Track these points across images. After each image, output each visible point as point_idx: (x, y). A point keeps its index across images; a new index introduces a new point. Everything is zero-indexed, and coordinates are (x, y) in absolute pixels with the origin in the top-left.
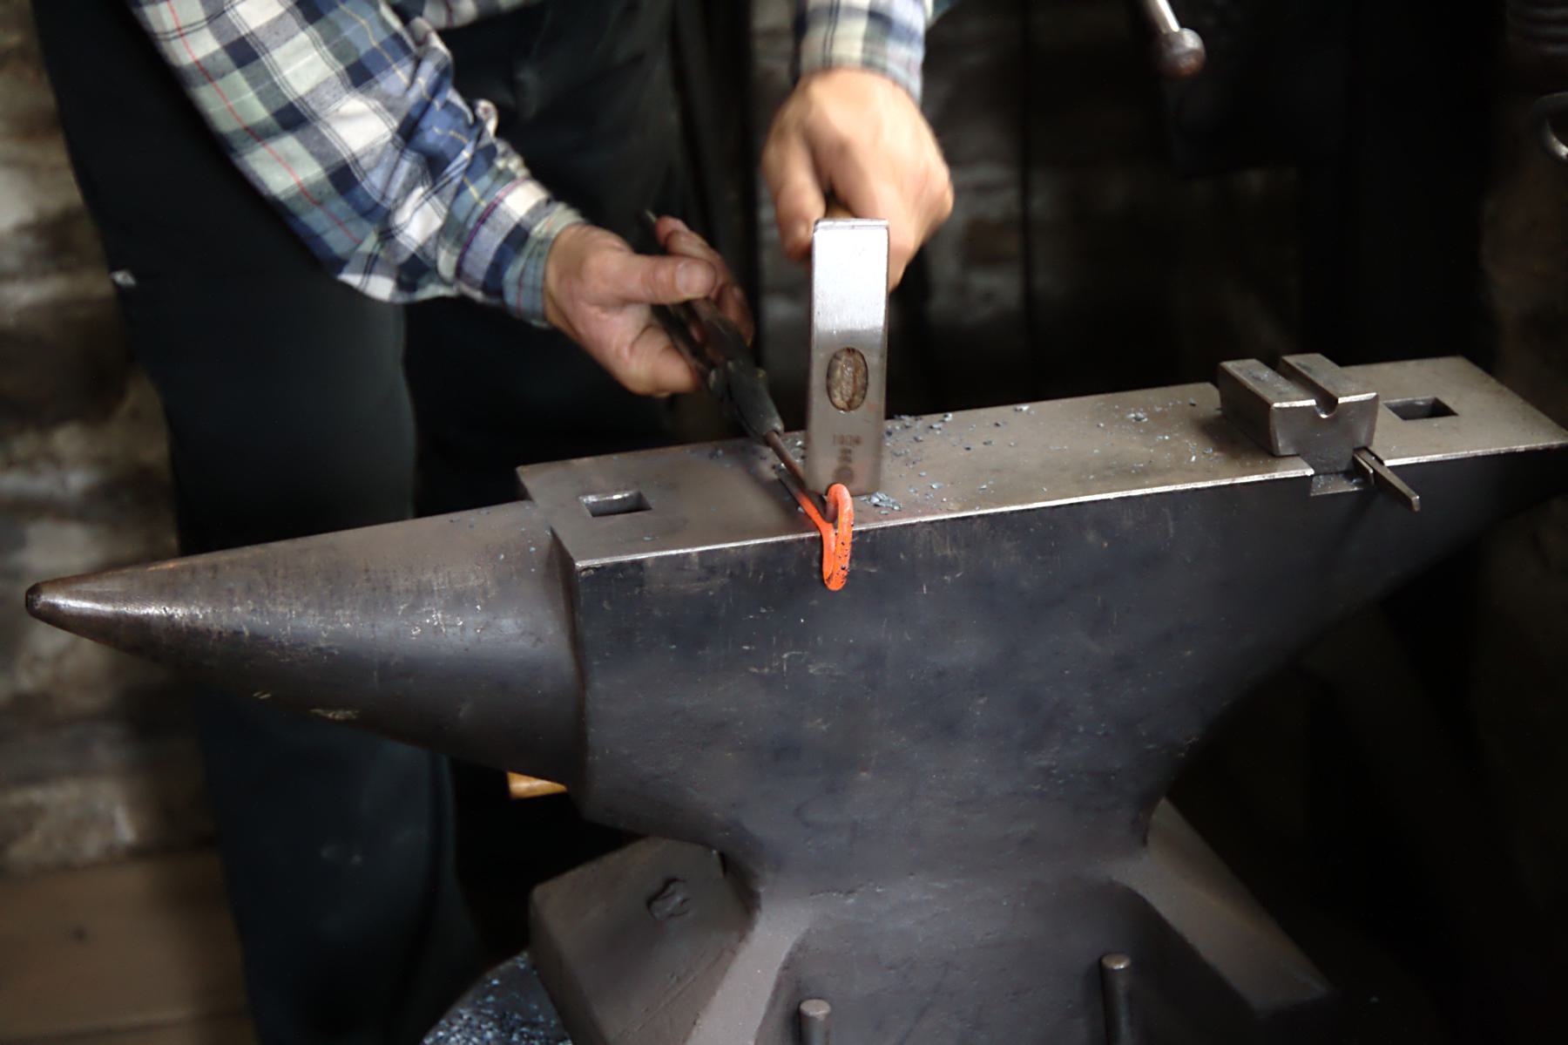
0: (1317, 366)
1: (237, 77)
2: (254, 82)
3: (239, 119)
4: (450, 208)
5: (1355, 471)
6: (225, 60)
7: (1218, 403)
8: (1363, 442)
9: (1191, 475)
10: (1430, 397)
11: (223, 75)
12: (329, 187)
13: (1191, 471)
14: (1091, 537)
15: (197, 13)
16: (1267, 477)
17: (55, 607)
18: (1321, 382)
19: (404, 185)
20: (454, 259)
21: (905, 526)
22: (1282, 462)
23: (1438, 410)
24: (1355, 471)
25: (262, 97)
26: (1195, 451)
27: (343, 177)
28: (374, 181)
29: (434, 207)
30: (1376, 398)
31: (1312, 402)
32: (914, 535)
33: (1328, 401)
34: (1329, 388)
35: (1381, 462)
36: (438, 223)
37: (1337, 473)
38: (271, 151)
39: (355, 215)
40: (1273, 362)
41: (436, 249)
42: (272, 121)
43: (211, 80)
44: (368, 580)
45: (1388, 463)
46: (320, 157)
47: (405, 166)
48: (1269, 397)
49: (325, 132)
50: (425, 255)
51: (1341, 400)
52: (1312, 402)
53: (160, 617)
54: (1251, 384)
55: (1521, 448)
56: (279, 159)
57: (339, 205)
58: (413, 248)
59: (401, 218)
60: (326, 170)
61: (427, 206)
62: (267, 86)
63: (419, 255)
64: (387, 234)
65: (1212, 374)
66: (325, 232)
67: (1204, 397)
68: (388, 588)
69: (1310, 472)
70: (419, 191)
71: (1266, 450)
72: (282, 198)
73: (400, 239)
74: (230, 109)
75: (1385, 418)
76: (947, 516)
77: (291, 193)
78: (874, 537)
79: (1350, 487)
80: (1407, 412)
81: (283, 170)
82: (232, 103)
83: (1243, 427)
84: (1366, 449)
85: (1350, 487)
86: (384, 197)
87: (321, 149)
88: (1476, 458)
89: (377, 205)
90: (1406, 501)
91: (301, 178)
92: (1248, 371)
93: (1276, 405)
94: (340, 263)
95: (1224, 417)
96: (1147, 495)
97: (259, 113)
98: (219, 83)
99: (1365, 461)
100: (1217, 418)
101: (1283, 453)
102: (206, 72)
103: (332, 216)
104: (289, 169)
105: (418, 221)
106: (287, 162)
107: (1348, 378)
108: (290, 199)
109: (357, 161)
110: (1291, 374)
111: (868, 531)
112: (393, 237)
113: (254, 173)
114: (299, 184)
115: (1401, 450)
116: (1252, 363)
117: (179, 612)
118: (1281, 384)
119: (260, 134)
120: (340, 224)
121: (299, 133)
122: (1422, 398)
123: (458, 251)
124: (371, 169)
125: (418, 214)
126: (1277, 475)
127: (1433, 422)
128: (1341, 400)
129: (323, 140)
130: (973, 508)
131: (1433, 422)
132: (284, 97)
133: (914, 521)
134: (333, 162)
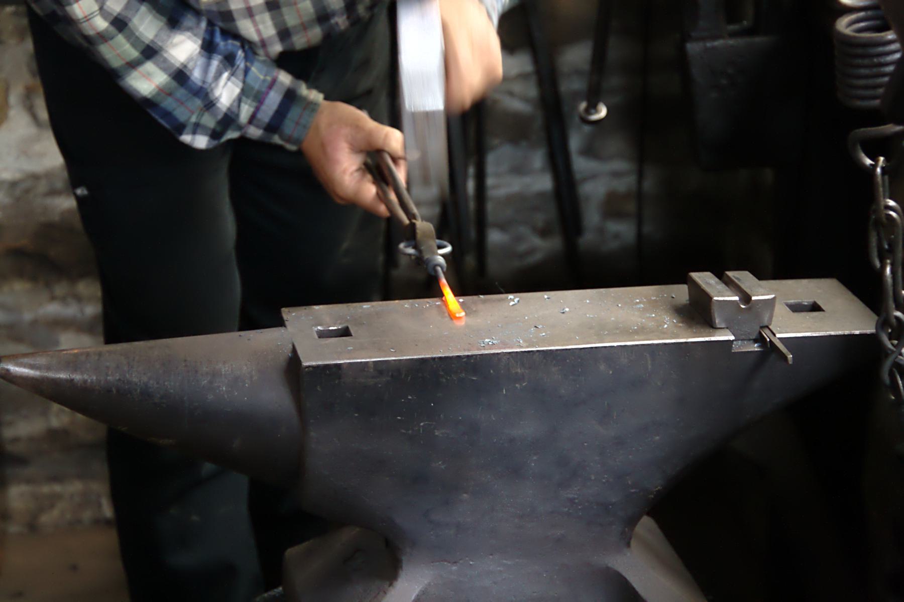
0: (745, 278)
1: (120, 38)
2: (128, 38)
3: (123, 59)
4: (244, 82)
5: (760, 339)
6: (112, 30)
7: (687, 297)
8: (766, 323)
9: (664, 334)
10: (811, 300)
11: (112, 38)
12: (174, 84)
13: (664, 333)
14: (602, 367)
15: (96, 7)
16: (707, 339)
17: (8, 370)
18: (743, 286)
19: (216, 73)
20: (252, 110)
21: (494, 354)
22: (718, 331)
23: (815, 308)
24: (760, 339)
25: (134, 45)
26: (669, 321)
27: (180, 76)
28: (196, 75)
29: (233, 83)
30: (774, 298)
31: (737, 298)
32: (499, 360)
33: (746, 298)
34: (748, 291)
35: (774, 335)
36: (237, 91)
37: (750, 340)
38: (140, 72)
39: (190, 95)
40: (720, 275)
41: (239, 106)
42: (141, 56)
43: (106, 41)
44: (186, 366)
45: (778, 336)
46: (164, 70)
47: (215, 63)
48: (712, 294)
49: (165, 55)
50: (232, 112)
51: (754, 298)
52: (737, 298)
53: (66, 380)
54: (704, 286)
55: (857, 332)
56: (144, 76)
57: (181, 92)
58: (224, 109)
59: (217, 93)
60: (170, 75)
61: (229, 84)
62: (134, 39)
63: (229, 114)
64: (210, 104)
65: (683, 279)
66: (174, 110)
67: (680, 293)
68: (196, 372)
69: (732, 338)
70: (226, 75)
71: (709, 324)
72: (149, 97)
73: (218, 105)
74: (119, 55)
75: (780, 310)
76: (518, 350)
77: (154, 93)
78: (476, 359)
79: (755, 347)
80: (796, 308)
81: (146, 82)
82: (119, 50)
83: (698, 312)
84: (767, 327)
85: (755, 347)
86: (204, 82)
87: (165, 65)
88: (831, 336)
89: (201, 88)
90: (785, 358)
91: (158, 83)
92: (705, 279)
93: (715, 298)
94: (181, 128)
95: (690, 304)
96: (605, 347)
97: (134, 54)
98: (111, 42)
99: (766, 334)
100: (685, 306)
101: (718, 326)
102: (103, 37)
103: (178, 100)
104: (150, 80)
105: (226, 92)
106: (148, 76)
107: (760, 286)
108: (154, 97)
109: (185, 66)
110: (730, 283)
111: (472, 356)
112: (214, 105)
113: (131, 86)
114: (157, 87)
115: (788, 329)
116: (708, 274)
117: (77, 377)
118: (721, 286)
119: (133, 65)
120: (182, 103)
121: (154, 59)
122: (806, 301)
123: (255, 104)
124: (193, 69)
125: (225, 89)
126: (713, 339)
127: (807, 314)
128: (754, 298)
129: (165, 60)
130: (533, 346)
131: (807, 314)
132: (143, 42)
133: (499, 351)
134: (172, 71)
